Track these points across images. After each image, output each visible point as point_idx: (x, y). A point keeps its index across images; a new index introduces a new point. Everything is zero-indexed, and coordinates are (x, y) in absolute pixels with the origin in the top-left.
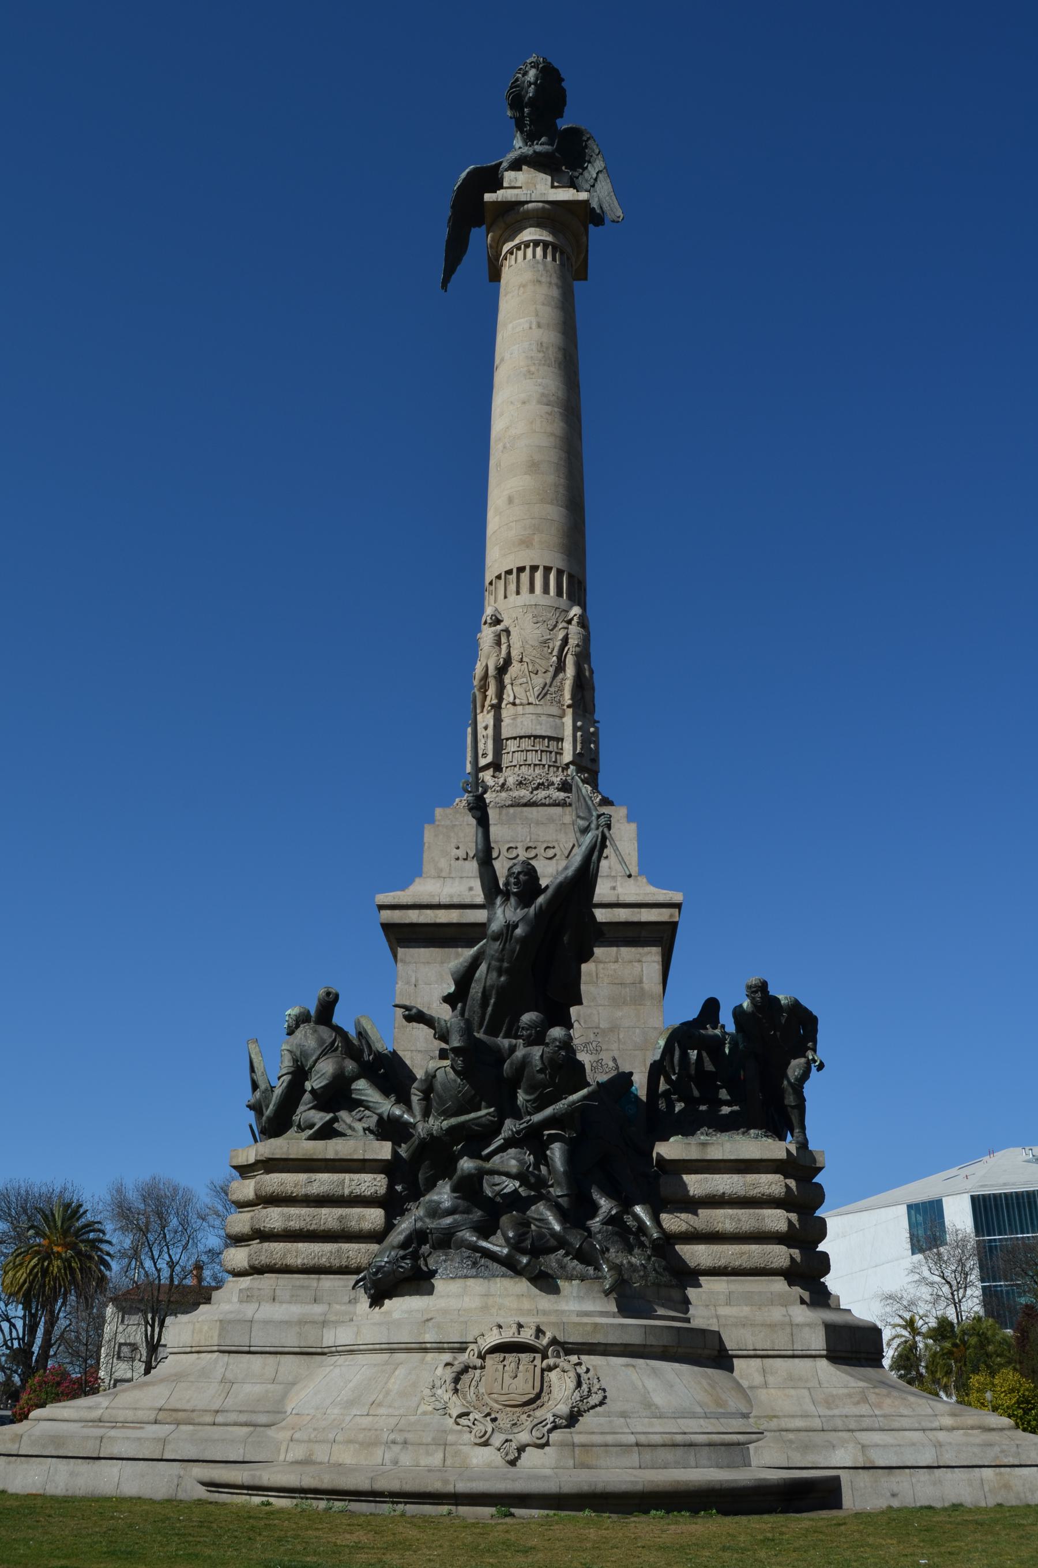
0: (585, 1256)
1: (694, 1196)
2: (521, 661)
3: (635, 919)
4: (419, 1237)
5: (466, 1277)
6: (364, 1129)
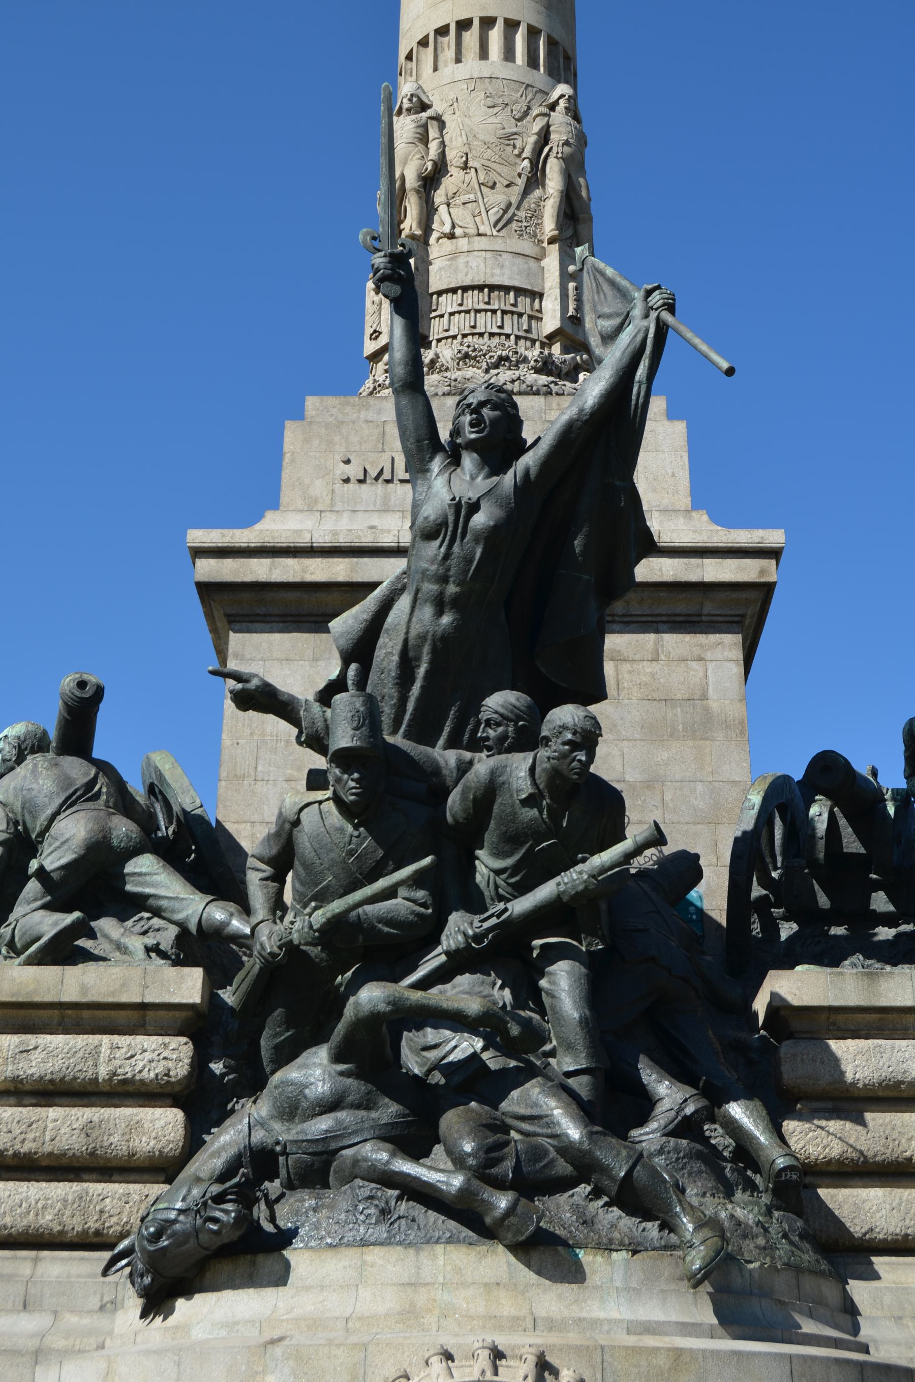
0: (638, 1198)
1: (854, 1084)
2: (465, 167)
3: (693, 577)
4: (260, 1161)
5: (364, 1243)
6: (148, 950)
